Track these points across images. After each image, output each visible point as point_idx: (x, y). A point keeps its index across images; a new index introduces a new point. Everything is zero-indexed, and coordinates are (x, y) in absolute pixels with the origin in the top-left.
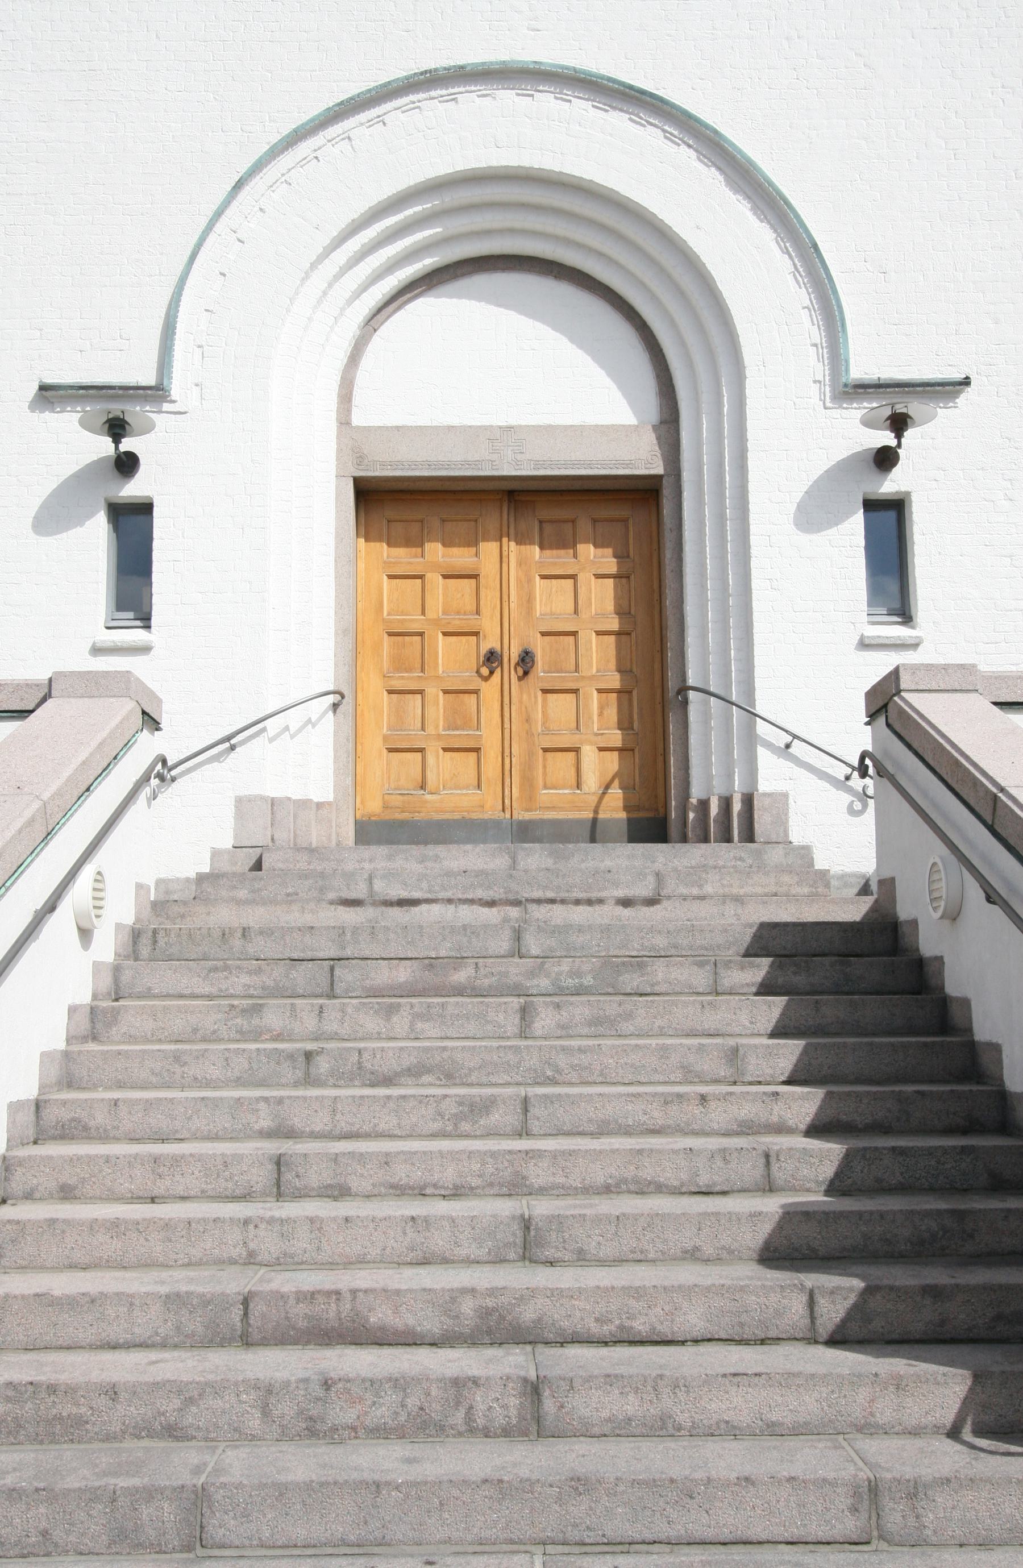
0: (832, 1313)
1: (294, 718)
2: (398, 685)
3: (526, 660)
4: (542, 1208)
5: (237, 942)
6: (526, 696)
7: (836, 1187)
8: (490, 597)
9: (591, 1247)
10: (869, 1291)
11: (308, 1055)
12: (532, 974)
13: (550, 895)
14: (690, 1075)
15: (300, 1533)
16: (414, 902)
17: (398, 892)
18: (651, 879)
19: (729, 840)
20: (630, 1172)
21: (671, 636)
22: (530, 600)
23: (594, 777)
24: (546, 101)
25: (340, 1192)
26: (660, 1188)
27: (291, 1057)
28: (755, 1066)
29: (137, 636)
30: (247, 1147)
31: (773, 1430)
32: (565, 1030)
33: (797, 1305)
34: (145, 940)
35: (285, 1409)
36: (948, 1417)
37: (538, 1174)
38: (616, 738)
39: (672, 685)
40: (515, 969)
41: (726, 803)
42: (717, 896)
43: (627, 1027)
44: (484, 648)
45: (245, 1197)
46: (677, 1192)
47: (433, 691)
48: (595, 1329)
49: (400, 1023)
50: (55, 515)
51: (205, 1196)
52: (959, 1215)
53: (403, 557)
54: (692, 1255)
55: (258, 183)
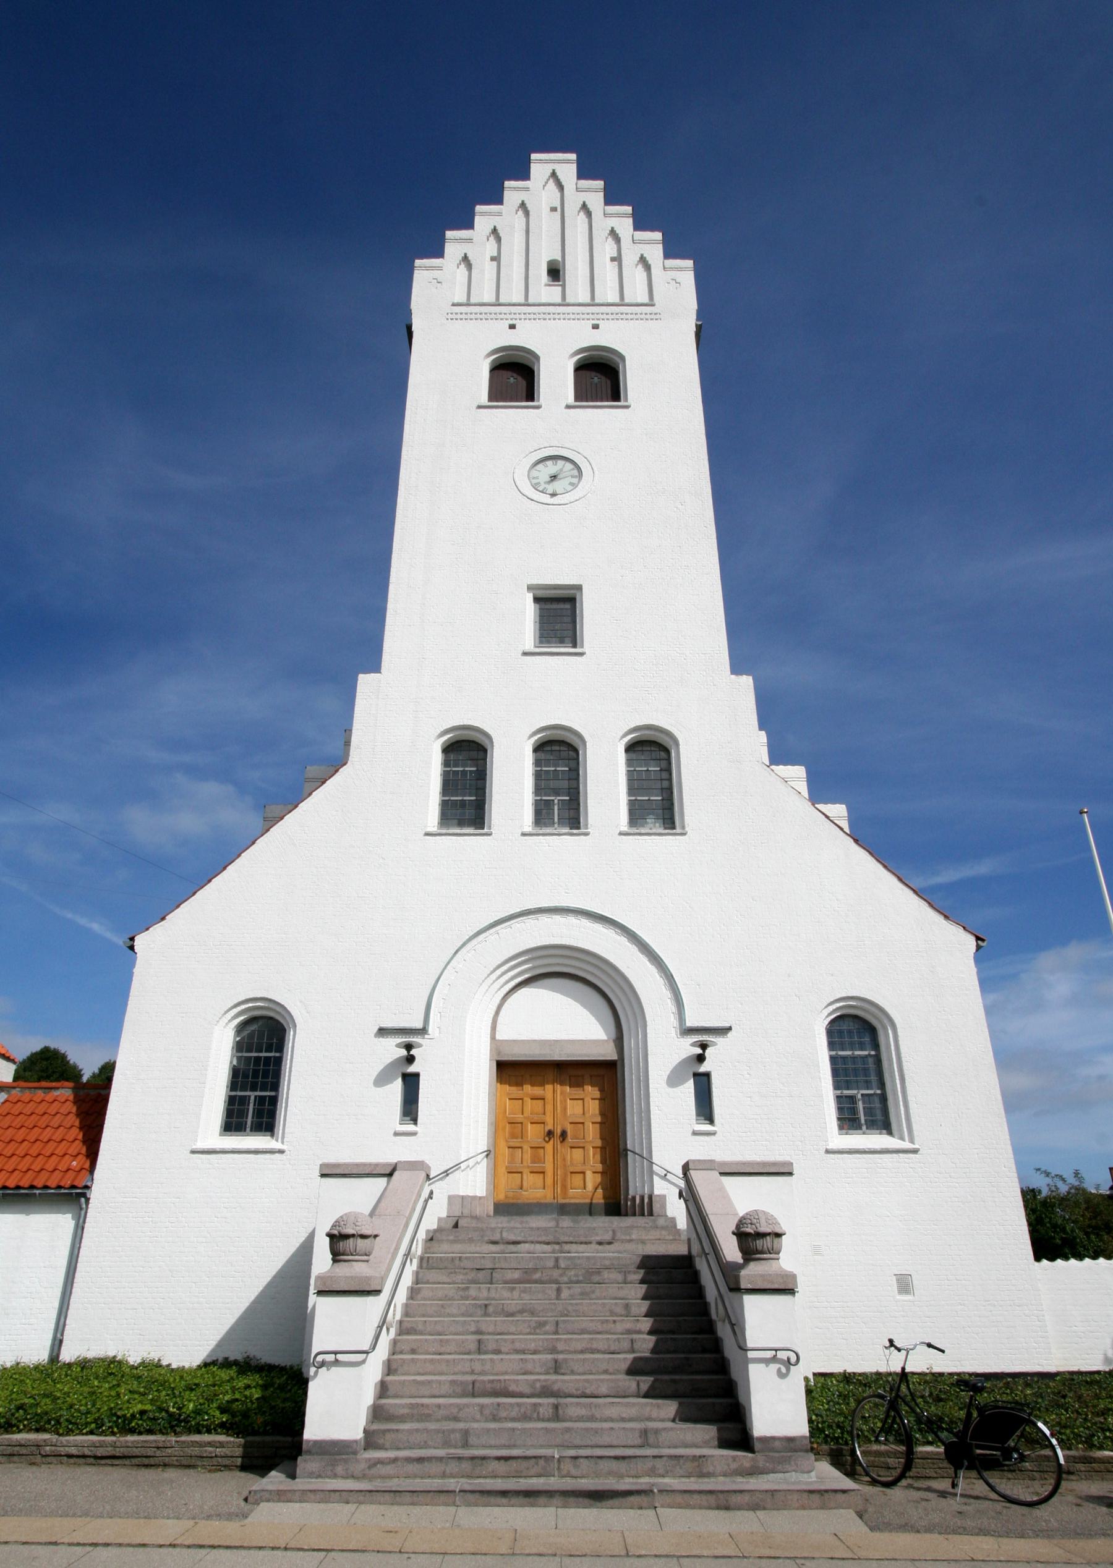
0: (644, 1387)
1: (471, 1162)
2: (512, 1144)
3: (564, 1134)
4: (561, 1357)
5: (457, 1262)
6: (564, 1150)
7: (653, 1351)
8: (549, 1107)
9: (575, 1368)
10: (654, 1382)
11: (486, 1306)
12: (561, 1275)
13: (571, 1239)
14: (612, 1313)
15: (493, 1443)
16: (518, 1243)
17: (512, 1238)
18: (611, 1233)
19: (643, 1215)
20: (589, 1346)
21: (621, 1126)
22: (565, 1109)
23: (588, 1185)
24: (572, 920)
25: (498, 1352)
26: (598, 1351)
27: (480, 1306)
28: (635, 1310)
29: (411, 1128)
30: (470, 1337)
31: (623, 1420)
32: (572, 1297)
33: (634, 1385)
34: (425, 1261)
35: (487, 1412)
36: (672, 1415)
37: (560, 1346)
38: (599, 1167)
39: (621, 1147)
40: (556, 1274)
41: (642, 1198)
42: (637, 1240)
43: (593, 1296)
44: (547, 1129)
45: (469, 1353)
46: (604, 1353)
47: (526, 1147)
48: (575, 1392)
49: (516, 1294)
50: (382, 1080)
51: (456, 1353)
52: (687, 1359)
53: (514, 1091)
54: (606, 1372)
55: (464, 950)
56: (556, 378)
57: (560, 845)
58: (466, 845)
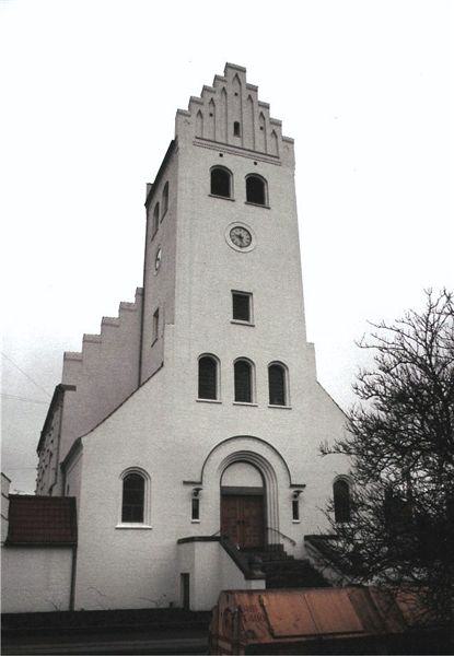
56: (239, 187)
57: (243, 410)
58: (206, 408)
